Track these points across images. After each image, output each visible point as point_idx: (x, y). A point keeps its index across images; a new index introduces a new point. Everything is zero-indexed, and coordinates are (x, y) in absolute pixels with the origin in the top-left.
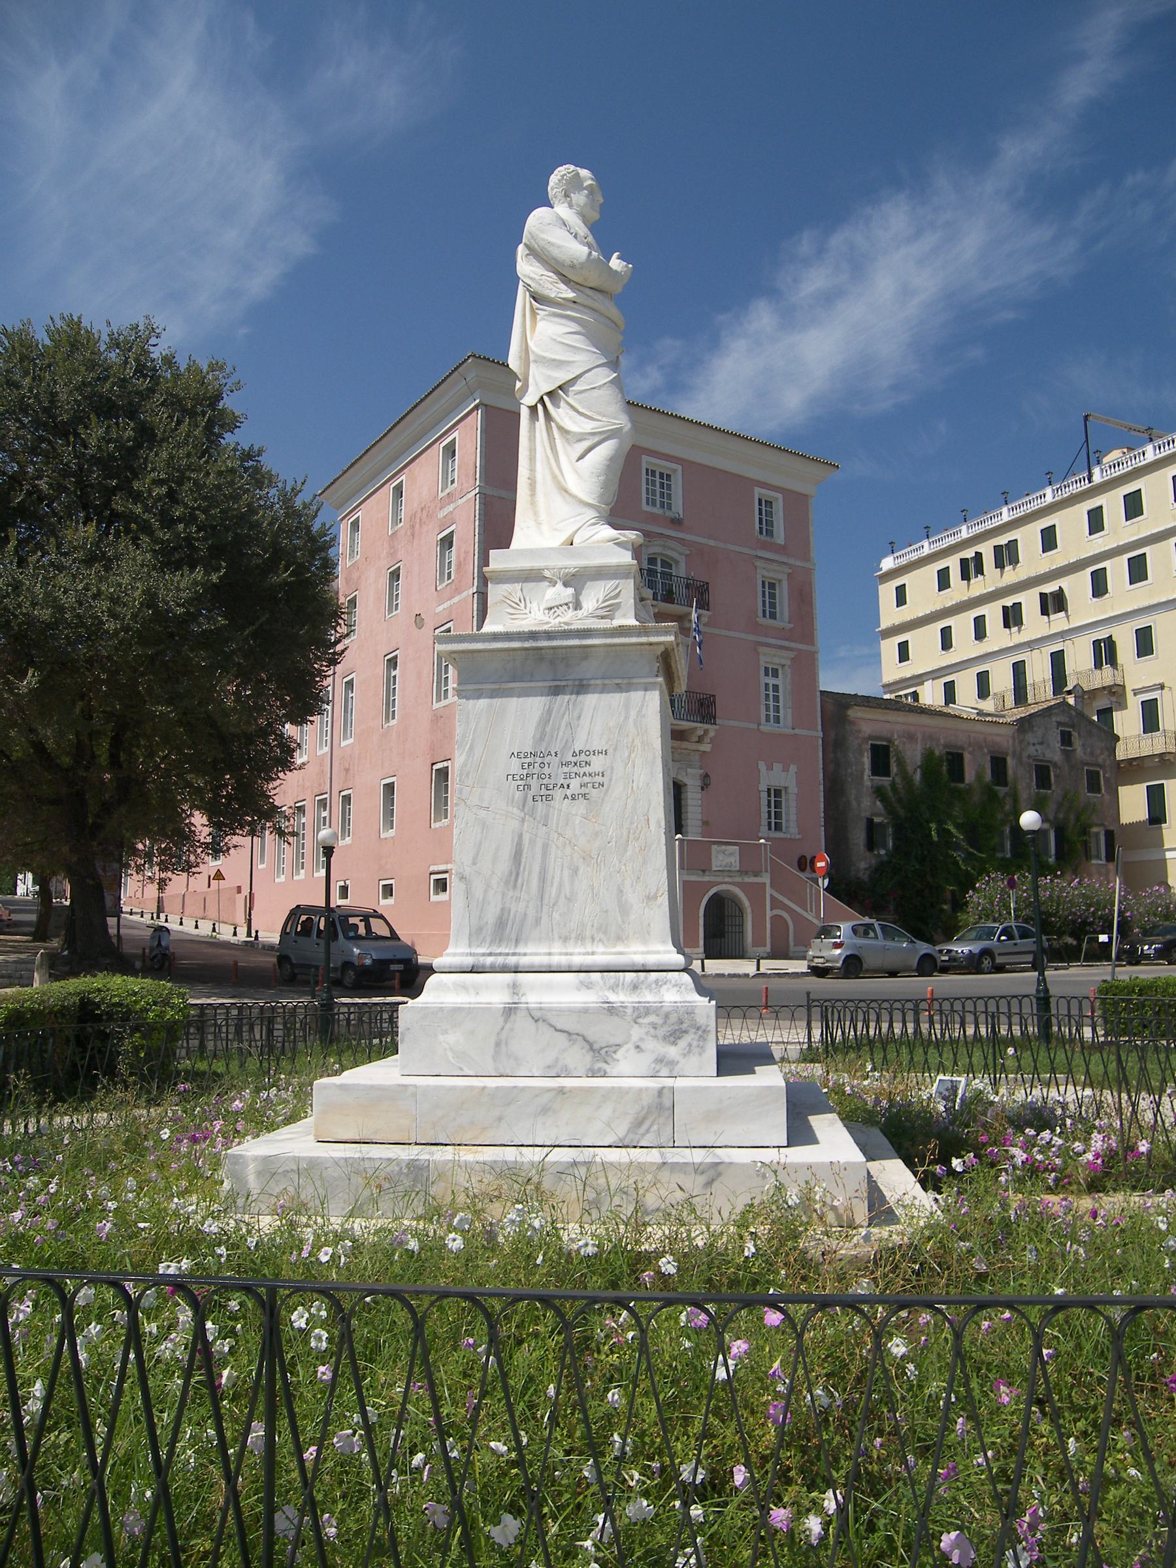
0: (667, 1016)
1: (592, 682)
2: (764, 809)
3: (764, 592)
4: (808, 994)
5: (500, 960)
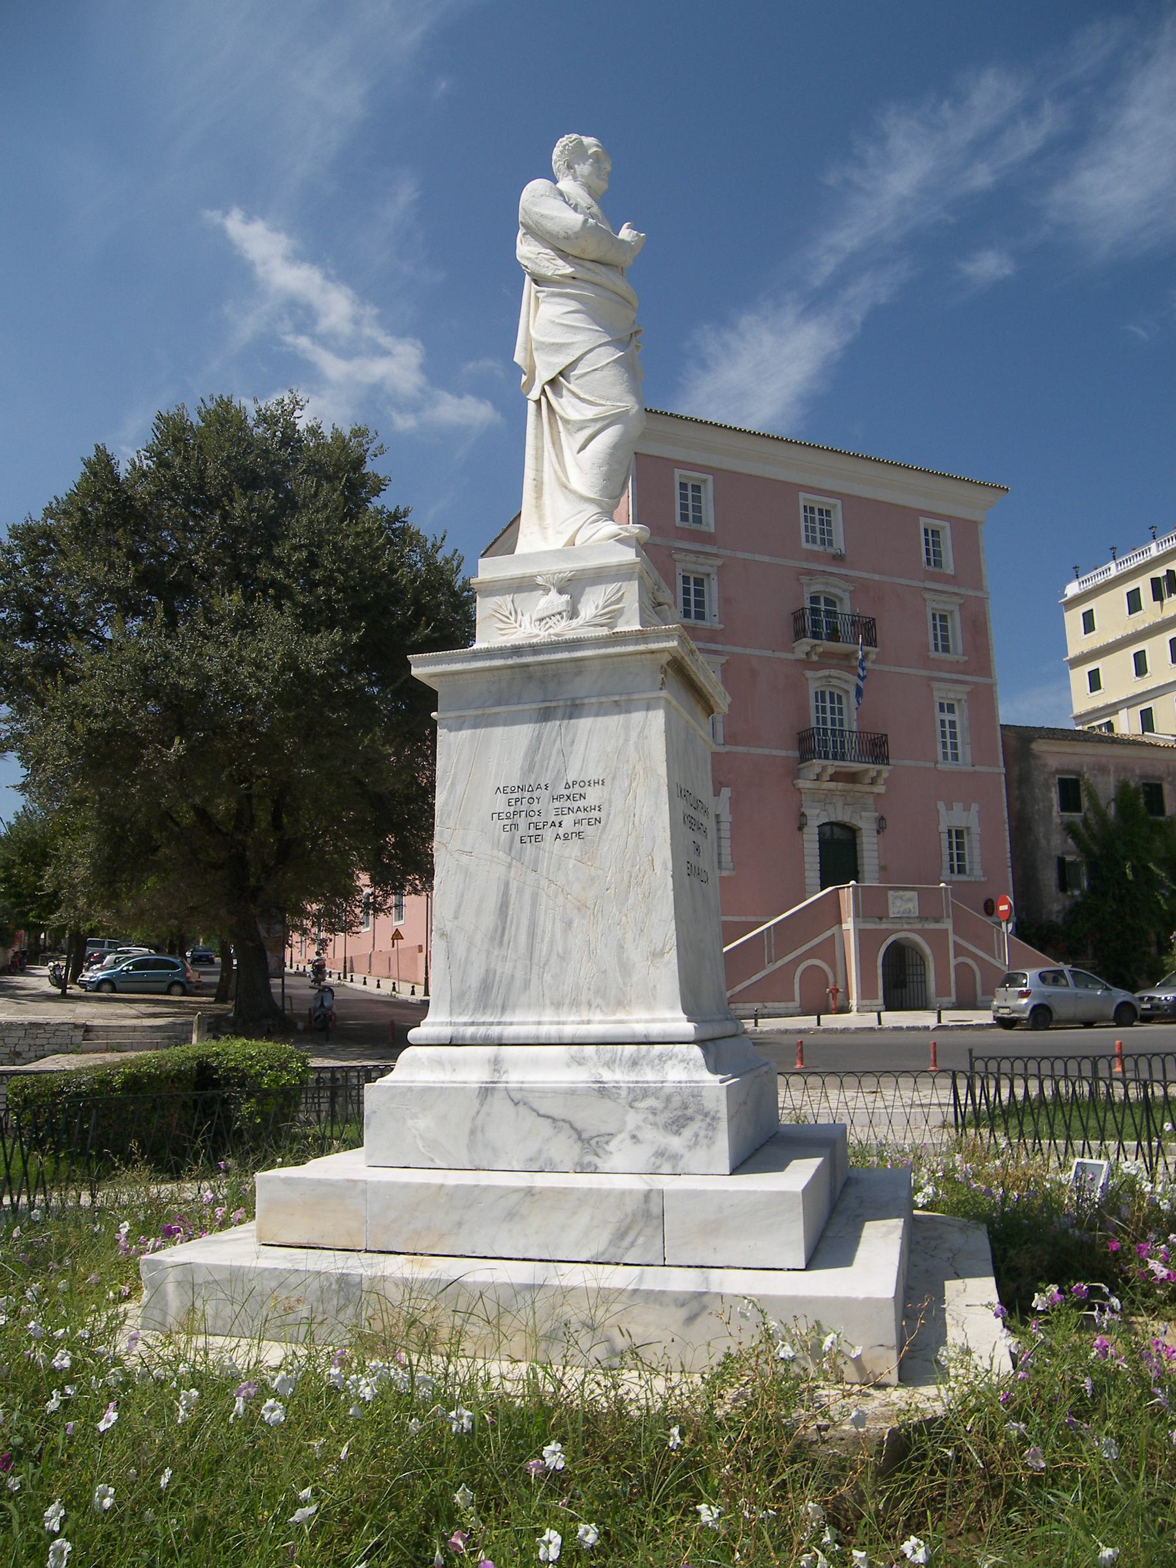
0: (668, 1099)
1: (586, 701)
2: (945, 851)
3: (935, 626)
4: (970, 1051)
5: (482, 1031)
